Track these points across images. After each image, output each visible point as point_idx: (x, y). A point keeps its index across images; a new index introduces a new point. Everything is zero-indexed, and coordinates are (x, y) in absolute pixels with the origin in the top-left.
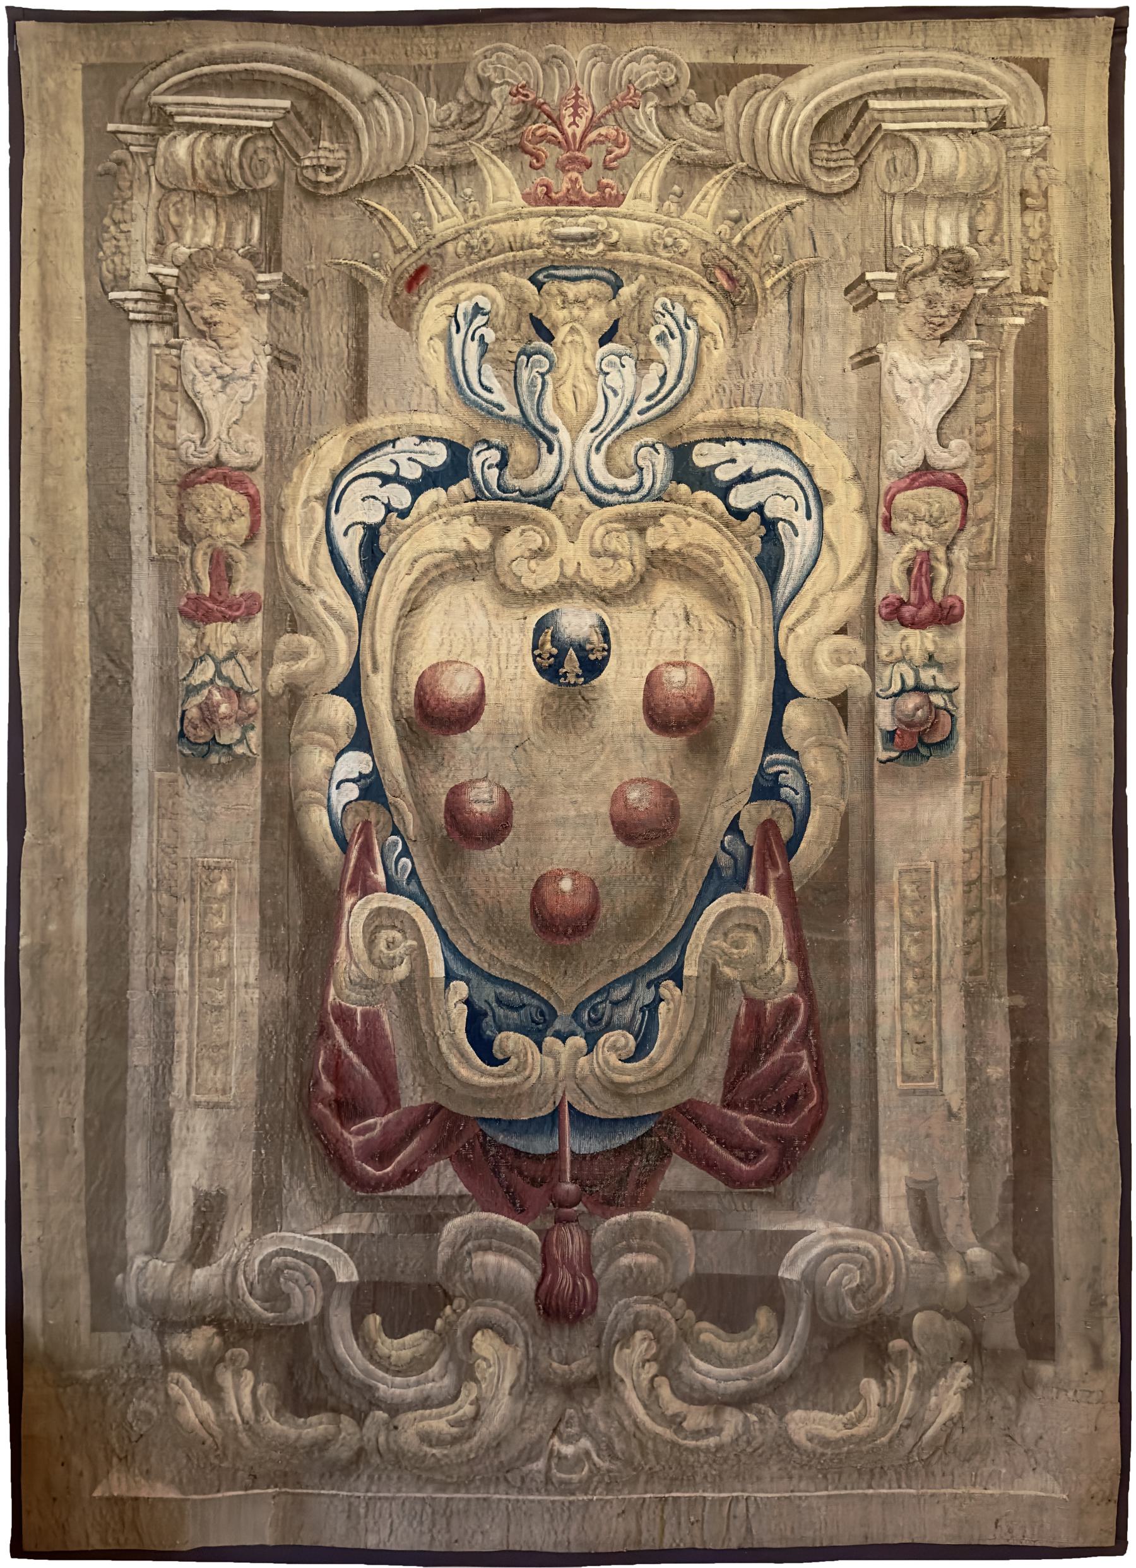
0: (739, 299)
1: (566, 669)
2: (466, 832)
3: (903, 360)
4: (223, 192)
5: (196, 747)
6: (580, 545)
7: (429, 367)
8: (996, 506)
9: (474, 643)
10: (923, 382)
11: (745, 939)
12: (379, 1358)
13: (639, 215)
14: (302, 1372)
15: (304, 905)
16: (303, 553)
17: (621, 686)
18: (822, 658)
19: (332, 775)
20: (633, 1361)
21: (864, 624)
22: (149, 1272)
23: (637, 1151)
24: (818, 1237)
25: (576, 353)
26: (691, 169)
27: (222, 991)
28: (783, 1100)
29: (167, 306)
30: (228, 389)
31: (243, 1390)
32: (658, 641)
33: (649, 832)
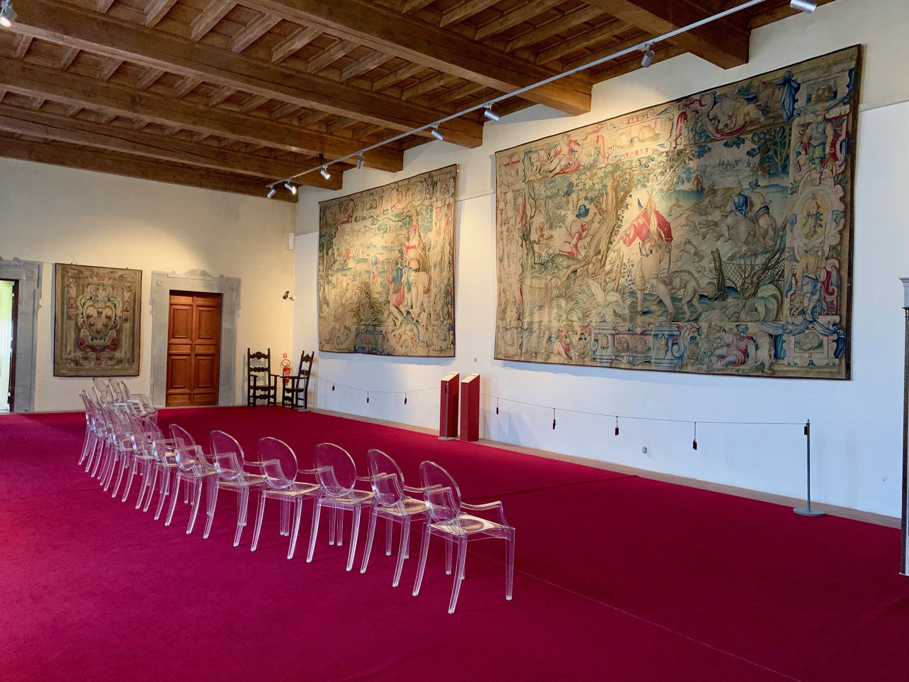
0: (113, 288)
1: (100, 313)
2: (91, 325)
3: (125, 293)
4: (73, 277)
5: (69, 318)
6: (100, 305)
7: (89, 291)
8: (132, 304)
9: (92, 311)
10: (127, 295)
11: (113, 333)
12: (84, 363)
13: (106, 281)
14: (77, 363)
15: (78, 330)
16: (79, 304)
17: (103, 315)
18: (119, 313)
19: (80, 321)
20: (103, 363)
21: (122, 311)
22: (64, 356)
23: (103, 349)
24: (117, 354)
25: (101, 290)
26: (109, 279)
27: (72, 335)
28: (115, 345)
29: (68, 286)
30: (73, 292)
31: (73, 365)
32: (107, 312)
33: (106, 326)
